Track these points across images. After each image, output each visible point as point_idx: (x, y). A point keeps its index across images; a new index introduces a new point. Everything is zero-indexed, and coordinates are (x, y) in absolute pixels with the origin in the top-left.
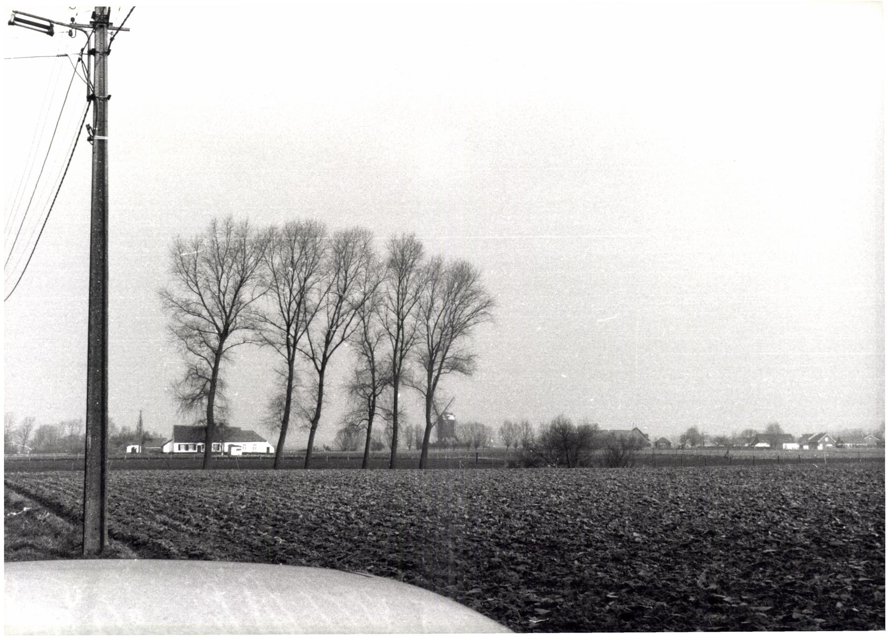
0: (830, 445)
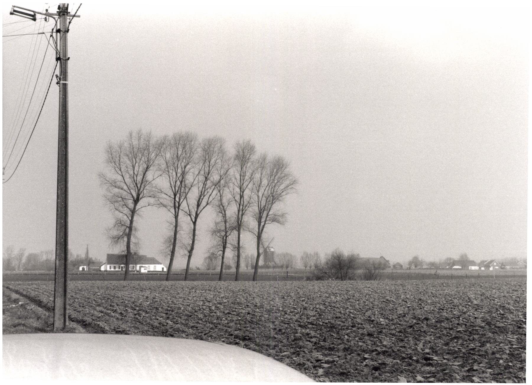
0: (497, 267)
